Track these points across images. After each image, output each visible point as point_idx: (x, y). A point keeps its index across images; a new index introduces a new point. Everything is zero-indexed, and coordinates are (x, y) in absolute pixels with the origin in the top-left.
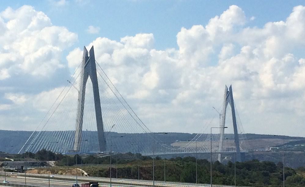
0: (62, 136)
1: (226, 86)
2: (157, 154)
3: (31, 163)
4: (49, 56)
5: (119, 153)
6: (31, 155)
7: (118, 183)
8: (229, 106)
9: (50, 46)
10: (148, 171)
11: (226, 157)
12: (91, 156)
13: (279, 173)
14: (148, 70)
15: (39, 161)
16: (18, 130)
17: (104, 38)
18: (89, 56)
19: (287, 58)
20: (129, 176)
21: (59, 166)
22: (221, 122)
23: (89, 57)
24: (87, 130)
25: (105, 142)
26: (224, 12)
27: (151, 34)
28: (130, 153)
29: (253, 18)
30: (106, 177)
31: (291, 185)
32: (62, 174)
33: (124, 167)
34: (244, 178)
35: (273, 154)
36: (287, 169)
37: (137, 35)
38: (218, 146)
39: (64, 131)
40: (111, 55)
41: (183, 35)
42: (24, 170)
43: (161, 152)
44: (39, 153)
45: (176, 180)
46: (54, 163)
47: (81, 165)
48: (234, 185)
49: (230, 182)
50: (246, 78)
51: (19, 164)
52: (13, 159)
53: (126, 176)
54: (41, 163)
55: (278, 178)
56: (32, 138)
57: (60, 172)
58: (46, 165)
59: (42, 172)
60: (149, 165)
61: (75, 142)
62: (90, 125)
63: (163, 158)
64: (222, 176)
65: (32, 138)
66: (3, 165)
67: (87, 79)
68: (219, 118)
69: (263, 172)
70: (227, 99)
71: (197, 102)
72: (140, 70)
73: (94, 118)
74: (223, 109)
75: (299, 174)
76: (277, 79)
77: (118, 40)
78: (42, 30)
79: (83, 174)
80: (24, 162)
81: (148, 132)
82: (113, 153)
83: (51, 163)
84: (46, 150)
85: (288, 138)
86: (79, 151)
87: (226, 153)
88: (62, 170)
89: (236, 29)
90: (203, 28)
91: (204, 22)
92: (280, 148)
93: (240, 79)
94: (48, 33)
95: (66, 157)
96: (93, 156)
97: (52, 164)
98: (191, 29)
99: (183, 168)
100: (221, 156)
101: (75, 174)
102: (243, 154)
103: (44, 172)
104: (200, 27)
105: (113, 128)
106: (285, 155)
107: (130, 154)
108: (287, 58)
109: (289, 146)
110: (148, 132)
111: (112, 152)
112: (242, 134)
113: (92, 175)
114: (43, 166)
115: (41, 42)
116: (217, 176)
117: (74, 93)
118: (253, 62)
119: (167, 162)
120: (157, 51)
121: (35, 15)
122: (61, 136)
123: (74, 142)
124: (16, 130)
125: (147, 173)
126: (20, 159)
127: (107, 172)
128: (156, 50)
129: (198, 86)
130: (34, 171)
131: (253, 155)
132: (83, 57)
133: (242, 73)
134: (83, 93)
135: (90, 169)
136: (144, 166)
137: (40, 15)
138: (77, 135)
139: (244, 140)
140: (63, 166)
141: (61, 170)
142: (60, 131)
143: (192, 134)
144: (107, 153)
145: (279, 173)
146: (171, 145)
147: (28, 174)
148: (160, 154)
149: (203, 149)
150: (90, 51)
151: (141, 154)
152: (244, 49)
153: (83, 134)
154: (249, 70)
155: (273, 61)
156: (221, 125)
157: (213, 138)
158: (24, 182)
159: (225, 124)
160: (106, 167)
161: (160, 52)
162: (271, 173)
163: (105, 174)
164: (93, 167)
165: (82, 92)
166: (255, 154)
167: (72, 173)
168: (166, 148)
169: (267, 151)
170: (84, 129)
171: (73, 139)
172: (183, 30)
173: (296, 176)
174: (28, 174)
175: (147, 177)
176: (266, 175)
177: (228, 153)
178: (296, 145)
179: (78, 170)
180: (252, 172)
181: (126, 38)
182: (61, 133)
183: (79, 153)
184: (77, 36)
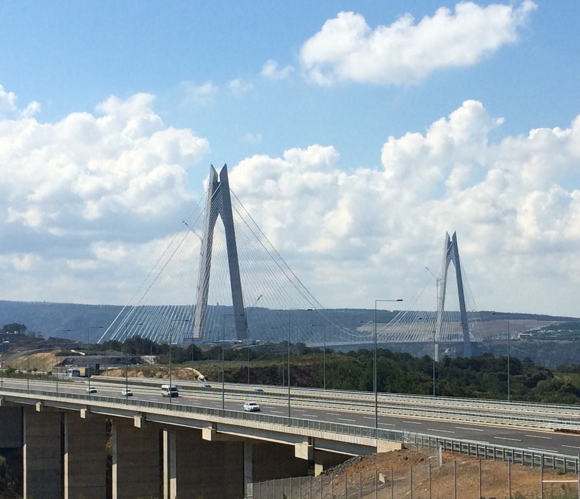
0: (184, 314)
1: (447, 233)
2: (328, 344)
3: (115, 358)
5: (268, 342)
6: (115, 345)
7: (248, 391)
8: (452, 266)
12: (217, 347)
13: (525, 376)
15: (130, 356)
16: (101, 304)
18: (219, 181)
20: (273, 381)
23: (219, 183)
24: (218, 303)
25: (246, 324)
30: (235, 382)
31: (545, 395)
32: (161, 377)
34: (468, 384)
35: (522, 344)
36: (540, 369)
37: (309, 147)
39: (176, 305)
43: (340, 341)
44: (129, 342)
45: (352, 387)
46: (154, 359)
48: (433, 395)
49: (442, 390)
50: (497, 221)
53: (268, 381)
55: (525, 384)
57: (158, 374)
58: (140, 362)
59: (129, 373)
62: (221, 296)
63: (337, 351)
66: (67, 361)
69: (500, 374)
70: (448, 254)
71: (412, 259)
76: (544, 221)
78: (151, 136)
79: (197, 377)
81: (317, 308)
82: (258, 342)
83: (148, 359)
84: (141, 337)
87: (448, 342)
90: (421, 137)
91: (422, 128)
92: (534, 335)
93: (487, 221)
94: (159, 143)
95: (175, 348)
101: (183, 377)
102: (474, 345)
103: (132, 374)
104: (417, 136)
109: (549, 331)
110: (315, 306)
111: (257, 341)
112: (474, 311)
114: (135, 364)
116: (421, 381)
117: (192, 244)
119: (339, 358)
122: (171, 313)
130: (116, 373)
131: (490, 346)
132: (210, 183)
135: (208, 370)
136: (300, 364)
138: (198, 311)
139: (476, 322)
141: (161, 370)
142: (170, 306)
143: (392, 311)
144: (248, 343)
145: (525, 376)
146: (359, 329)
147: (105, 377)
149: (411, 337)
150: (221, 173)
155: (536, 194)
157: (428, 317)
159: (446, 295)
160: (236, 365)
164: (215, 366)
166: (493, 344)
168: (351, 336)
169: (514, 340)
170: (445, 310)
173: (553, 380)
174: (105, 377)
177: (451, 342)
179: (189, 370)
183: (197, 344)
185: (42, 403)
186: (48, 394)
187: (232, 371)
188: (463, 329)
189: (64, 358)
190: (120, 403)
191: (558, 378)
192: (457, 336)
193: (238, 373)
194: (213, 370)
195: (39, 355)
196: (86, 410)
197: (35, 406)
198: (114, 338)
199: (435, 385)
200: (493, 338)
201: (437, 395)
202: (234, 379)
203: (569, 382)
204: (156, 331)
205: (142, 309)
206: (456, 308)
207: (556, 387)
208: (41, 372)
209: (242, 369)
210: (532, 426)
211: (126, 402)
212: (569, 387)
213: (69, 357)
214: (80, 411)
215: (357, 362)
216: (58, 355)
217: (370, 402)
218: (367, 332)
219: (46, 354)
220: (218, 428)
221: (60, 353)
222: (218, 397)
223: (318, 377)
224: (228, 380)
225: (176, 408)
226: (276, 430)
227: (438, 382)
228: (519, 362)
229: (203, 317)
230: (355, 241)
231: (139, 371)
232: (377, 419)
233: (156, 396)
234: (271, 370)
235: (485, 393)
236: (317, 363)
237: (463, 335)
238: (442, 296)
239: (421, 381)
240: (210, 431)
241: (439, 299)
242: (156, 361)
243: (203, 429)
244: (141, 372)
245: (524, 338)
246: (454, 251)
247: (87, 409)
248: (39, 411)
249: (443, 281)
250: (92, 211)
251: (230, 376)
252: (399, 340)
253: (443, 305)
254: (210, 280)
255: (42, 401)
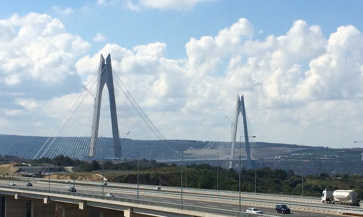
4: (60, 61)
6: (46, 160)
8: (241, 115)
9: (62, 52)
10: (167, 177)
11: (237, 165)
13: (290, 180)
14: (157, 78)
15: (57, 167)
17: (114, 45)
18: (106, 63)
19: (294, 69)
20: (148, 182)
21: (77, 171)
22: (233, 131)
23: (106, 65)
24: (101, 136)
25: (120, 148)
26: (234, 24)
27: (164, 43)
28: (145, 159)
29: (261, 32)
32: (81, 179)
33: (143, 173)
35: (282, 162)
36: (298, 177)
37: (149, 44)
38: (230, 154)
40: (119, 63)
41: (191, 45)
42: (42, 175)
44: (56, 158)
46: (72, 169)
47: (99, 170)
49: (245, 188)
50: (251, 89)
51: (37, 169)
52: (30, 164)
54: (59, 168)
56: (48, 144)
57: (80, 178)
58: (64, 170)
60: (167, 172)
61: (91, 148)
64: (237, 183)
65: (48, 144)
66: (21, 170)
67: (103, 88)
68: (231, 127)
70: (238, 108)
71: (206, 110)
72: (151, 78)
73: (119, 124)
74: (236, 118)
75: (308, 182)
76: (281, 91)
77: (131, 49)
80: (42, 167)
81: (162, 140)
82: (128, 159)
85: (295, 146)
86: (95, 157)
88: (82, 175)
89: (243, 39)
91: (215, 34)
95: (83, 163)
96: (110, 162)
97: (70, 170)
98: (201, 40)
99: (200, 174)
100: (233, 163)
101: (94, 180)
103: (63, 178)
104: (210, 37)
105: (128, 135)
106: (293, 163)
107: (145, 160)
108: (294, 69)
109: (297, 154)
111: (127, 158)
112: (253, 142)
113: (111, 181)
115: (52, 48)
118: (260, 73)
120: (167, 60)
121: (50, 22)
122: (76, 142)
123: (90, 148)
124: (30, 136)
125: (165, 179)
126: (38, 164)
127: (126, 178)
128: (166, 59)
129: (206, 95)
132: (100, 65)
133: (247, 83)
134: (99, 100)
137: (55, 23)
138: (92, 141)
140: (81, 172)
141: (81, 175)
144: (122, 160)
146: (185, 152)
148: (176, 160)
150: (107, 59)
151: (156, 161)
152: (251, 61)
153: (98, 141)
154: (254, 81)
155: (278, 72)
156: (233, 133)
157: (226, 145)
158: (48, 188)
160: (126, 173)
161: (170, 61)
162: (283, 180)
163: (124, 180)
164: (112, 173)
165: (98, 98)
166: (264, 161)
167: (92, 179)
169: (277, 159)
171: (88, 145)
172: (193, 40)
175: (166, 184)
176: (277, 182)
178: (304, 154)
179: (98, 176)
180: (264, 179)
181: (138, 47)
182: (76, 139)
184: (91, 45)
185: (18, 194)
186: (31, 190)
187: (124, 176)
188: (247, 153)
189: (19, 168)
190: (86, 196)
191: (309, 182)
192: (243, 157)
193: (127, 178)
194: (112, 176)
195: (4, 166)
196: (47, 198)
197: (14, 196)
198: (43, 156)
199: (241, 186)
200: (264, 158)
201: (219, 189)
202: (125, 181)
203: (315, 185)
204: (66, 151)
205: (60, 139)
206: (243, 140)
207: (308, 187)
208: (15, 177)
209: (129, 175)
210: (308, 209)
211: (13, 188)
212: (315, 187)
213: (22, 167)
214: (43, 200)
215: (195, 172)
216: (15, 166)
217: (179, 192)
218: (189, 154)
219: (8, 165)
220: (134, 210)
221: (16, 165)
222: (135, 192)
223: (173, 180)
224: (121, 182)
225: (77, 195)
226: (151, 209)
227: (242, 184)
228: (286, 173)
229: (95, 144)
230: (171, 100)
231: (68, 176)
232: (182, 201)
233: (64, 189)
234: (146, 176)
235: (267, 191)
236: (172, 172)
237: (247, 156)
238: (235, 133)
239: (233, 183)
240: (129, 212)
241: (233, 135)
242: (73, 170)
243: (125, 211)
244: (69, 177)
245: (283, 158)
246: (242, 107)
247: (48, 198)
248: (17, 199)
249: (236, 124)
250: (13, 80)
251: (122, 180)
252: (209, 158)
253: (235, 138)
254: (99, 123)
255: (18, 193)
